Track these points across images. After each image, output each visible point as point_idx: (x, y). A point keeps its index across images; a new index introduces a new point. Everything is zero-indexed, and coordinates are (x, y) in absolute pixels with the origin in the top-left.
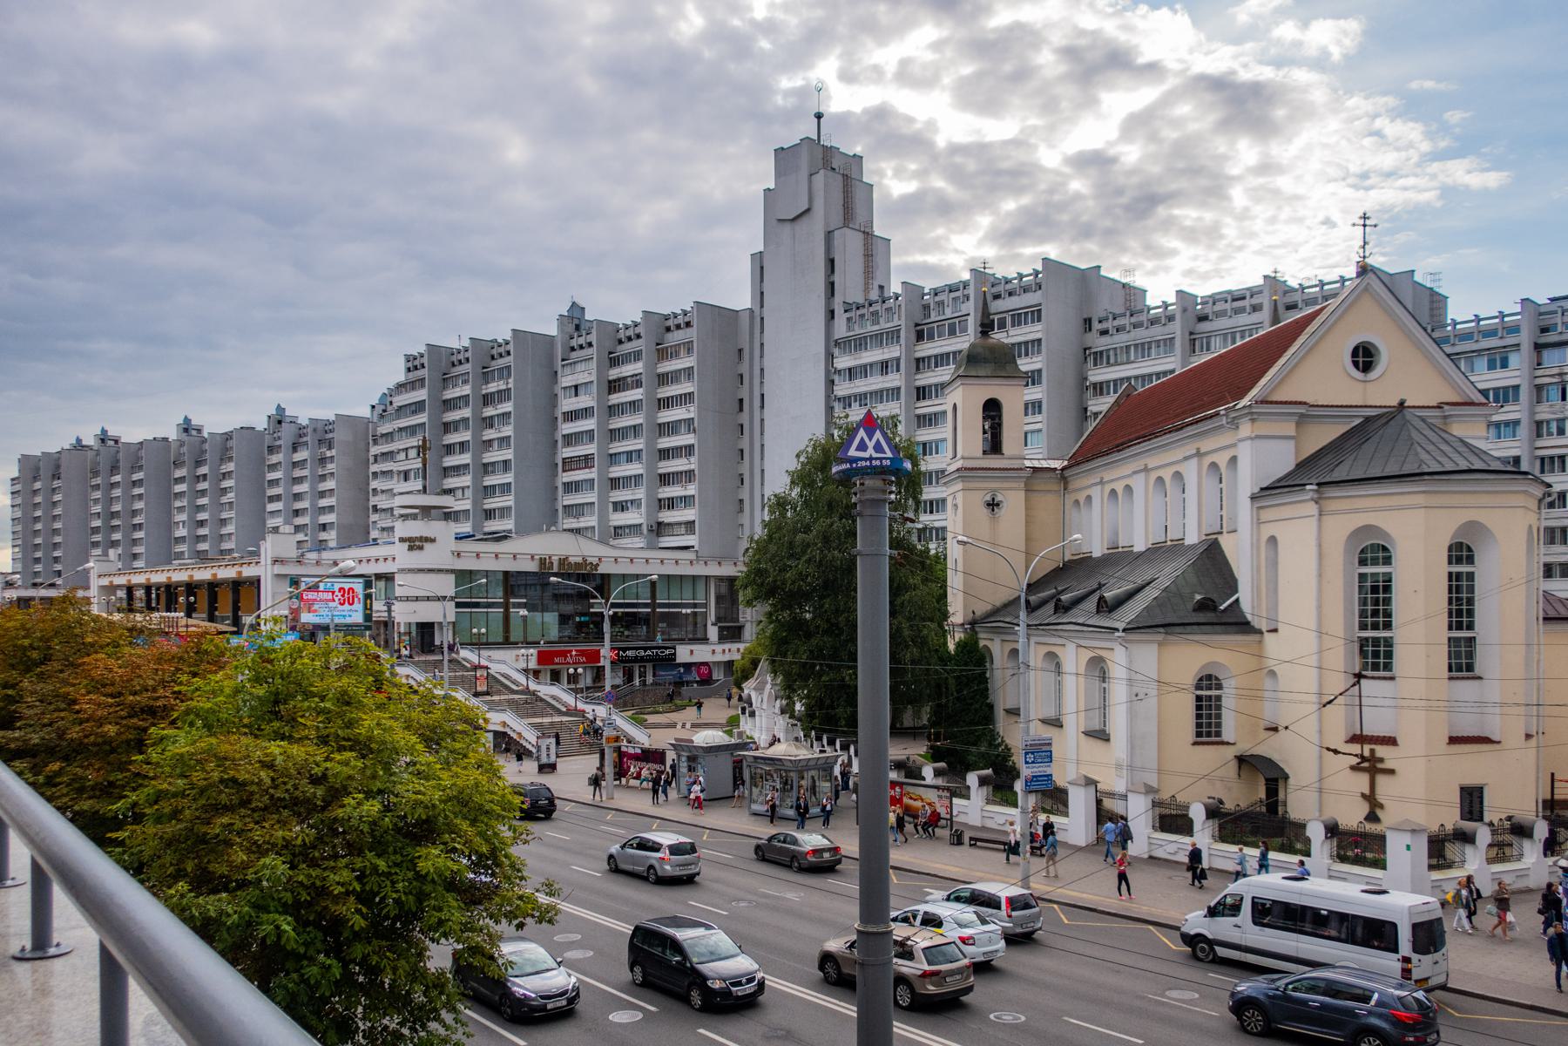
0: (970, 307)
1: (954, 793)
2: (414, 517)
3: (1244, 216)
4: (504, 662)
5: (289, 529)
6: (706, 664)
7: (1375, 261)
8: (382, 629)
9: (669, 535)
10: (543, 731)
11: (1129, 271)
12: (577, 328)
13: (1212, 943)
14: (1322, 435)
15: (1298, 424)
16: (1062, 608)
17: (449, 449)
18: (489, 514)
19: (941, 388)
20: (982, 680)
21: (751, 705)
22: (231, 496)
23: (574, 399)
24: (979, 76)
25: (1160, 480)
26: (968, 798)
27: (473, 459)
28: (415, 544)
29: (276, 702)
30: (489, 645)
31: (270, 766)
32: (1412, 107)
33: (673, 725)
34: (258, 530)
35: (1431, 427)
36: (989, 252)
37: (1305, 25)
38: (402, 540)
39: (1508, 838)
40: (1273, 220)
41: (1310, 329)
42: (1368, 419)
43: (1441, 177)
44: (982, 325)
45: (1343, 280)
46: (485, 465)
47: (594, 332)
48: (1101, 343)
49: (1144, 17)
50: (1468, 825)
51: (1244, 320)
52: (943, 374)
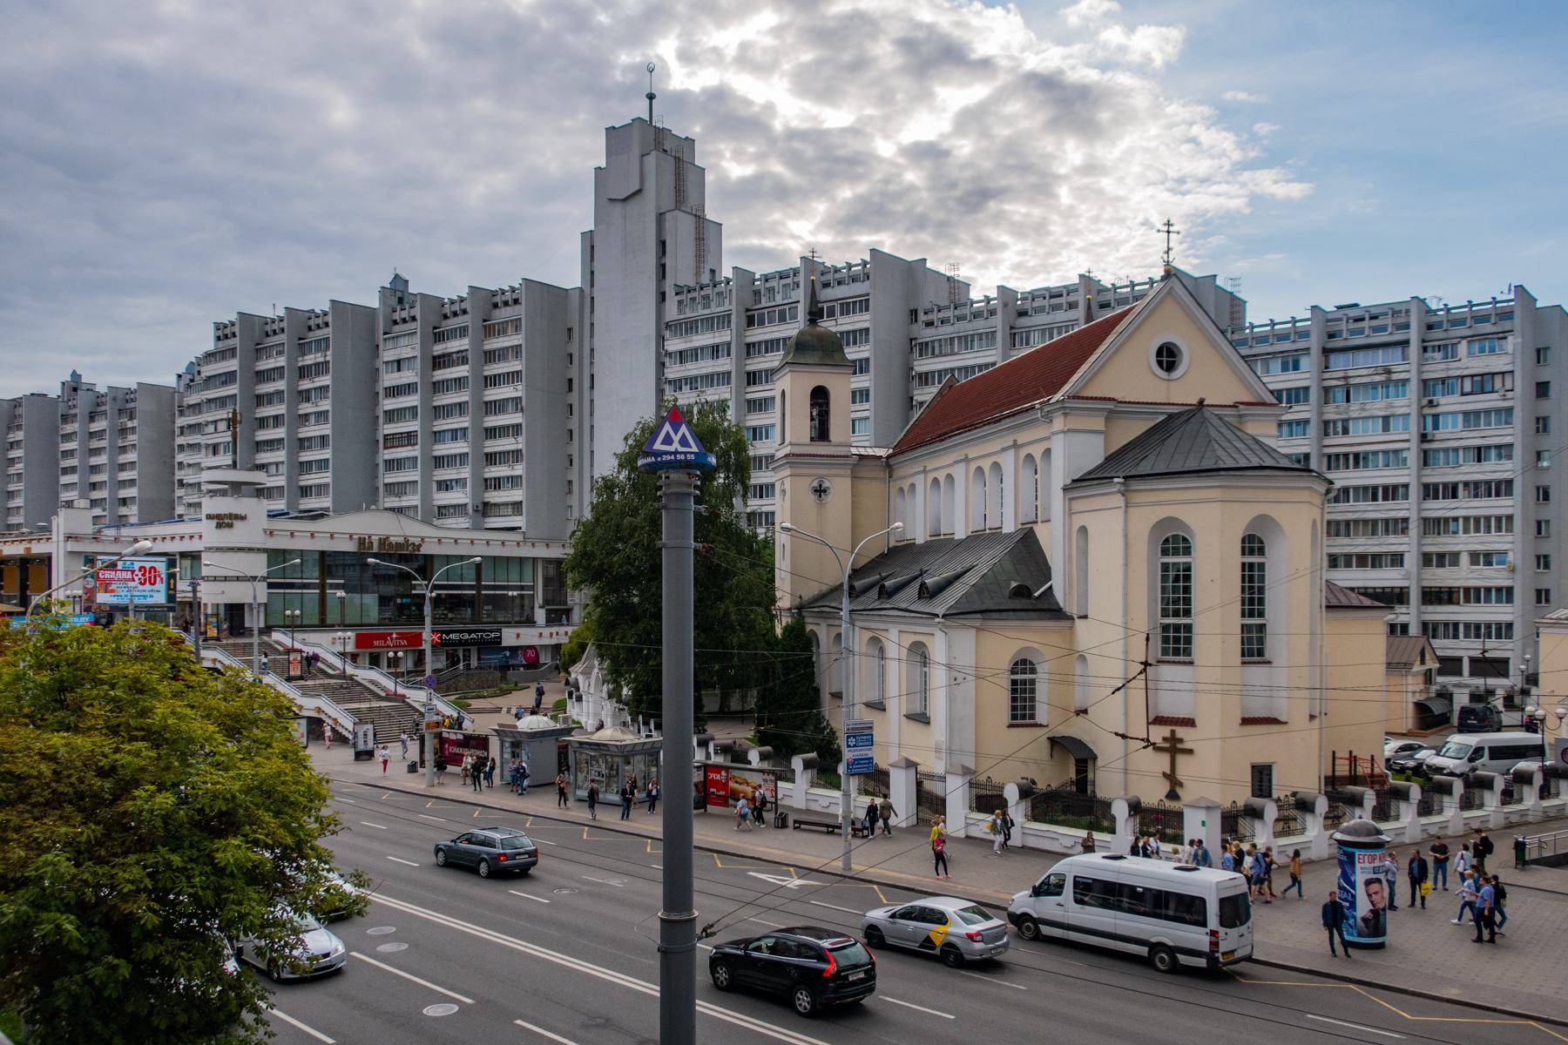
0: (800, 295)
1: (779, 777)
2: (224, 493)
3: (1069, 213)
4: (320, 645)
5: (84, 503)
6: (532, 647)
7: (1181, 264)
8: (186, 612)
9: (486, 514)
10: (360, 718)
11: (954, 266)
12: (401, 301)
13: (1037, 922)
14: (1132, 430)
15: (1107, 419)
16: (886, 594)
17: (262, 423)
18: (305, 491)
19: (770, 374)
20: (809, 664)
21: (578, 689)
22: (19, 467)
23: (396, 375)
24: (819, 63)
25: (980, 469)
26: (1113, 831)
27: (288, 433)
28: (224, 521)
29: (62, 690)
30: (303, 627)
31: (52, 758)
32: (1226, 116)
33: (498, 710)
34: (50, 504)
35: (1228, 425)
36: (825, 238)
37: (1130, 29)
38: (209, 517)
39: (1293, 812)
40: (1096, 219)
41: (1118, 329)
42: (1171, 416)
43: (1251, 186)
44: (810, 313)
45: (1151, 282)
46: (301, 440)
47: (418, 305)
48: (927, 335)
49: (979, 14)
50: (1258, 802)
51: (1061, 316)
52: (773, 360)
